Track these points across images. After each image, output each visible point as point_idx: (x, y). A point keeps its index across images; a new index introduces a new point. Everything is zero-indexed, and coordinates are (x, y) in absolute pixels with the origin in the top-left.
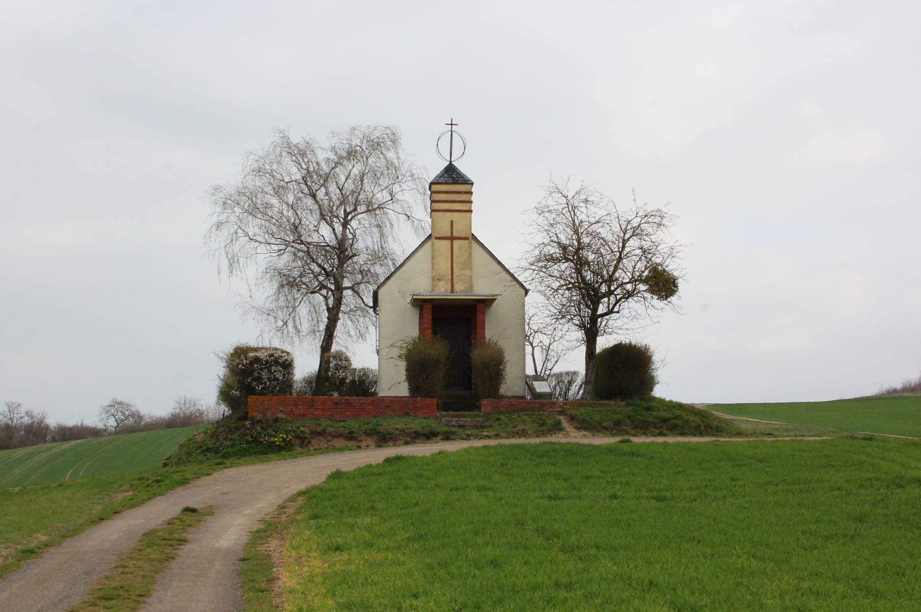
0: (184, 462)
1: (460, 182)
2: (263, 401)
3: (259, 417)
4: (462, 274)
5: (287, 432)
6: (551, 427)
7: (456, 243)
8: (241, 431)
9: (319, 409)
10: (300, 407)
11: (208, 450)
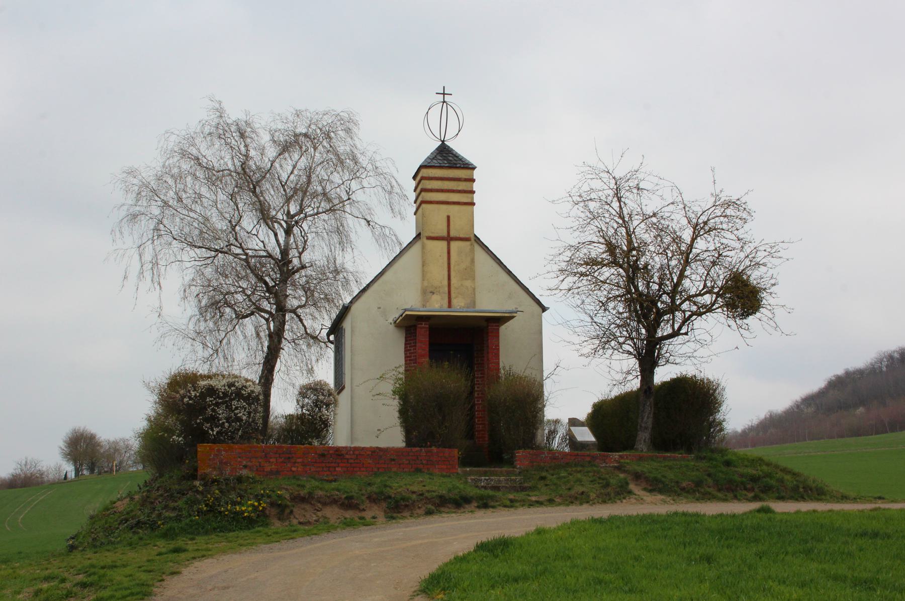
0: (102, 544)
1: (458, 165)
2: (219, 450)
3: (214, 475)
4: (462, 285)
5: (258, 498)
6: (618, 489)
7: (454, 245)
8: (188, 495)
9: (298, 463)
10: (271, 460)
11: (139, 524)
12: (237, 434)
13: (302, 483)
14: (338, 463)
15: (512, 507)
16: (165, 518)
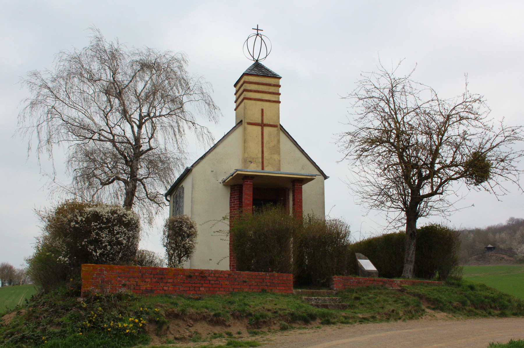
1: (269, 75)
2: (101, 270)
3: (97, 292)
4: (271, 157)
5: (138, 315)
7: (266, 129)
10: (147, 280)
12: (118, 256)
13: (175, 301)
14: (202, 284)
15: (348, 323)
16: (50, 333)
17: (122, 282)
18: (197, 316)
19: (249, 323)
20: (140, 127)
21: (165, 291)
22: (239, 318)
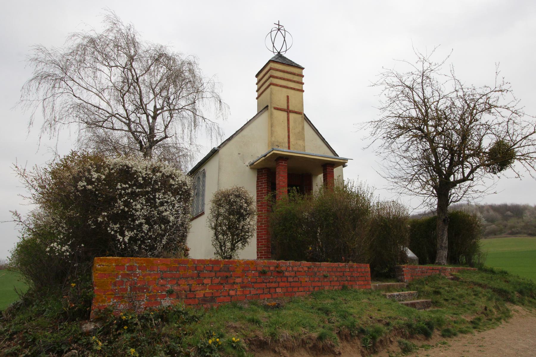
7: (292, 115)
10: (205, 281)
12: (161, 242)
17: (166, 287)
18: (293, 342)
19: (363, 347)
20: (154, 118)
21: (231, 297)
22: (349, 338)
